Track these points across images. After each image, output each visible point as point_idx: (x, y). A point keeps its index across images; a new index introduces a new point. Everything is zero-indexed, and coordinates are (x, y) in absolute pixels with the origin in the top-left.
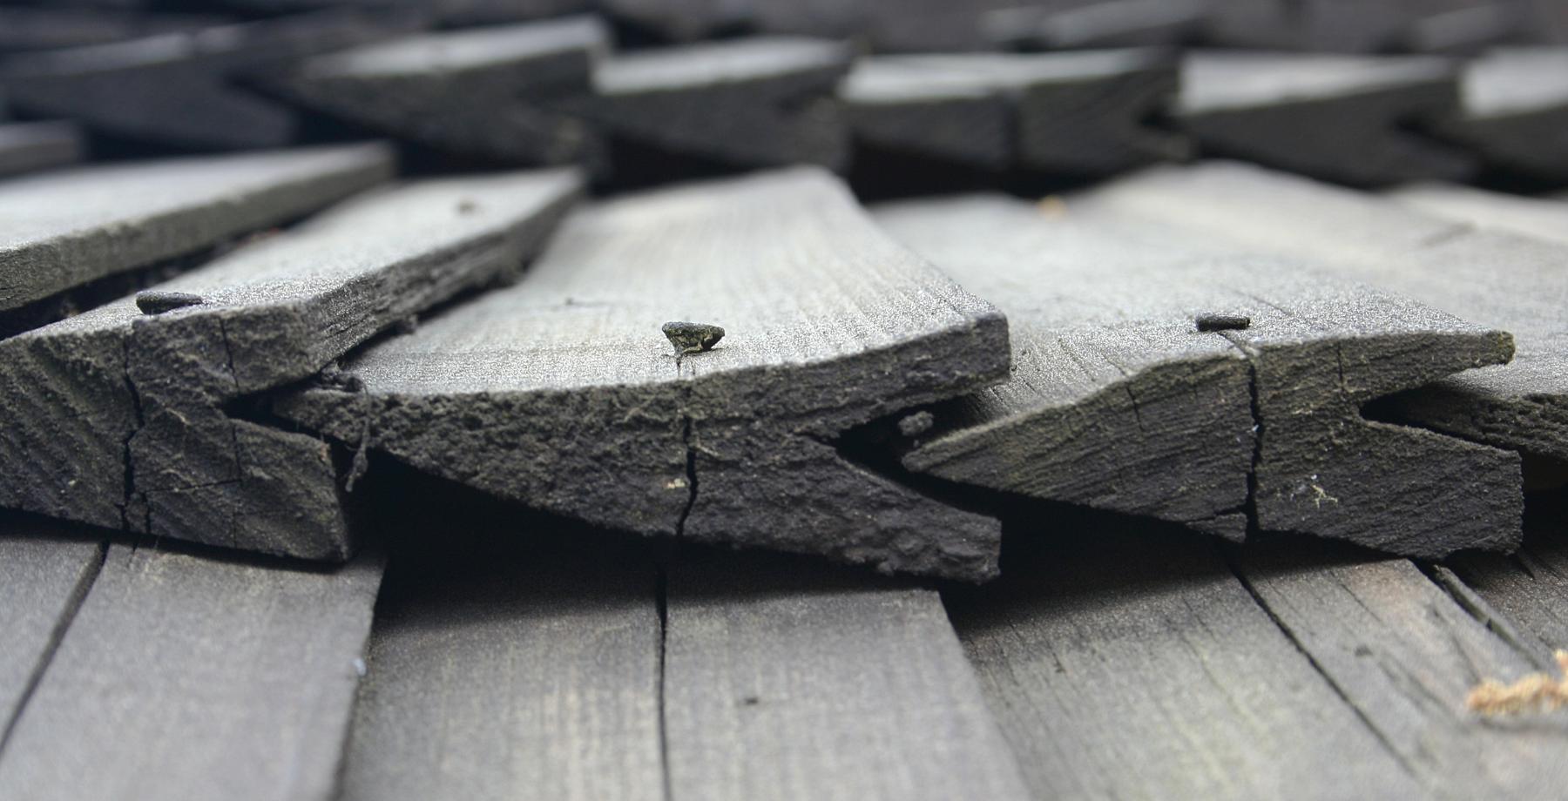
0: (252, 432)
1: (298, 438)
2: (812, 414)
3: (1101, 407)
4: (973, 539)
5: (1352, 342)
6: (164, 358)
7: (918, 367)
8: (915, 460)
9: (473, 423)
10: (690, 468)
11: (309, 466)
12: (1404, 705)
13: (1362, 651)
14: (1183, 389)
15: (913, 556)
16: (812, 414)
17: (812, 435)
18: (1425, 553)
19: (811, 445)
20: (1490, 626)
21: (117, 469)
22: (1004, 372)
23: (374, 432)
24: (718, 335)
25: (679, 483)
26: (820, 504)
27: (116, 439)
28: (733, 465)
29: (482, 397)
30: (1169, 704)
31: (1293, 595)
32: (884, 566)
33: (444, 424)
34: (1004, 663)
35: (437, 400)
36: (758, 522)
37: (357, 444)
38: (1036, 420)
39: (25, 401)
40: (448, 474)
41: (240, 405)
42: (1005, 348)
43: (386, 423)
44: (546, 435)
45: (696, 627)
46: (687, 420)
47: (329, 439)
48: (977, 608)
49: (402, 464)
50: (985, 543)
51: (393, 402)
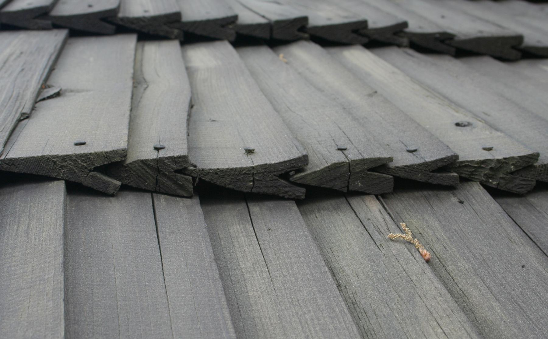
0: (179, 176)
1: (187, 177)
2: (274, 172)
3: (324, 171)
4: (301, 192)
5: (367, 159)
6: (164, 164)
7: (293, 164)
8: (291, 179)
9: (216, 174)
10: (253, 181)
11: (189, 181)
12: (377, 233)
13: (369, 219)
14: (337, 167)
15: (291, 195)
16: (274, 172)
17: (274, 175)
18: (377, 194)
19: (274, 177)
20: (389, 214)
21: (155, 181)
22: (307, 164)
23: (199, 175)
24: (254, 150)
25: (251, 183)
26: (276, 187)
27: (155, 176)
28: (261, 180)
29: (218, 169)
30: (337, 228)
31: (355, 202)
32: (286, 197)
33: (212, 174)
34: (306, 215)
35: (211, 169)
36: (265, 190)
37: (197, 178)
38: (313, 173)
39: (139, 170)
40: (212, 182)
41: (177, 171)
42: (308, 160)
43: (202, 173)
44: (229, 176)
45: (255, 209)
46: (253, 173)
47: (192, 176)
48: (300, 203)
49: (204, 181)
50: (303, 193)
51: (203, 170)
